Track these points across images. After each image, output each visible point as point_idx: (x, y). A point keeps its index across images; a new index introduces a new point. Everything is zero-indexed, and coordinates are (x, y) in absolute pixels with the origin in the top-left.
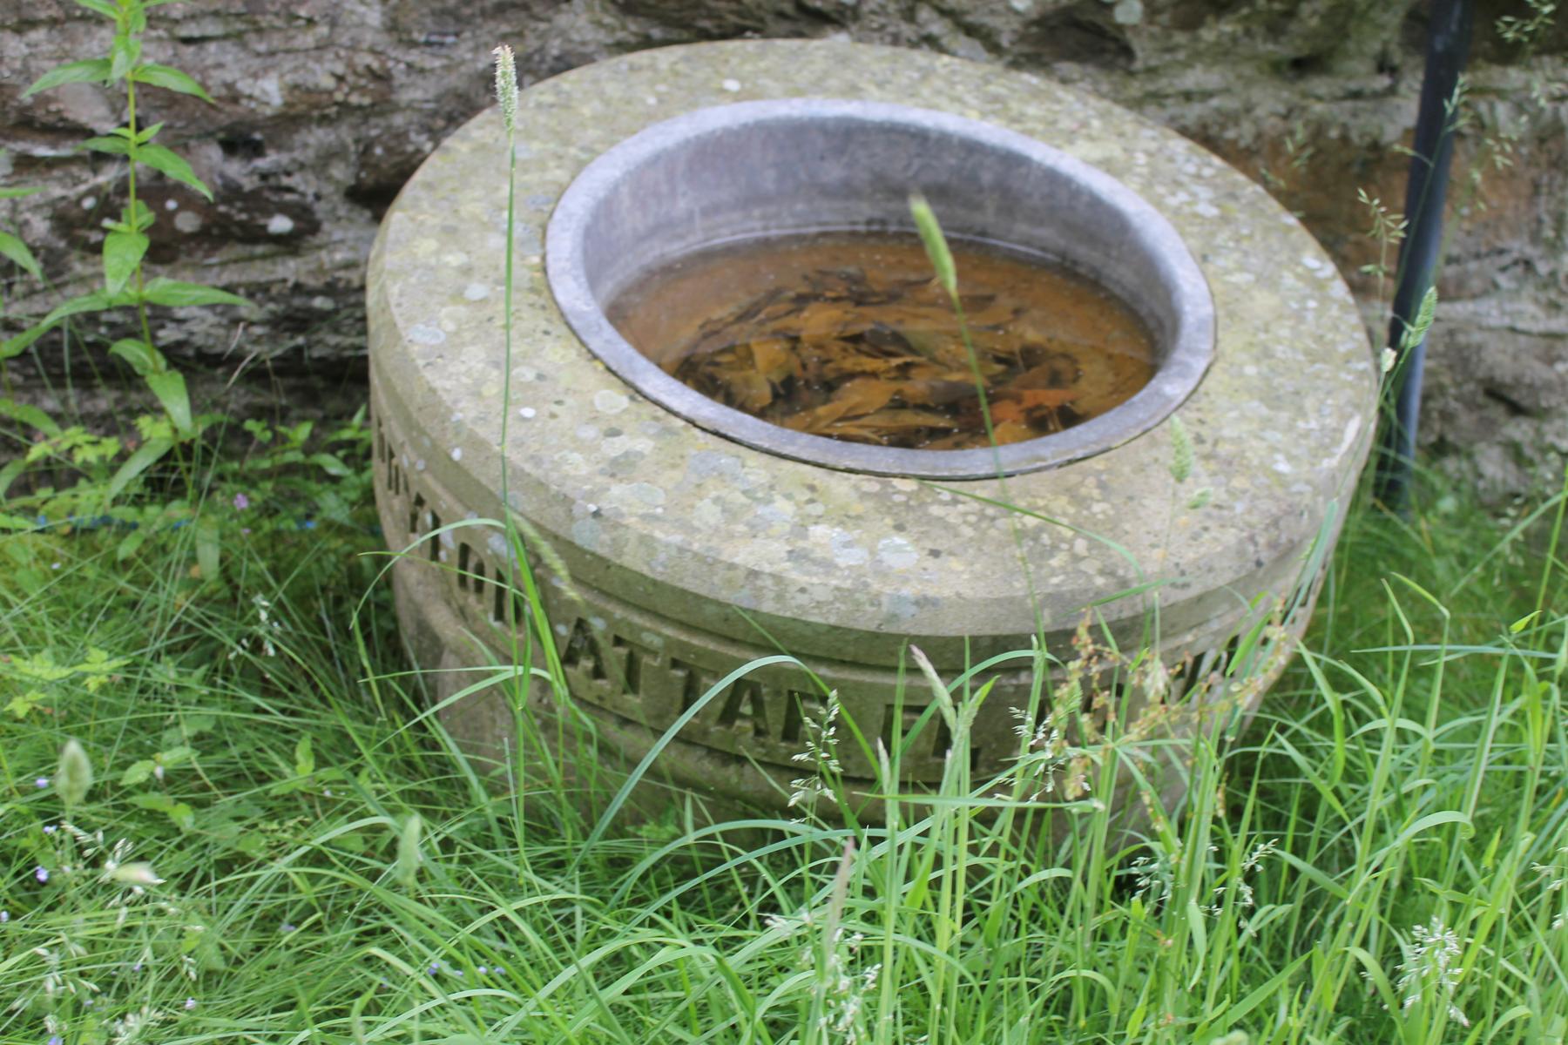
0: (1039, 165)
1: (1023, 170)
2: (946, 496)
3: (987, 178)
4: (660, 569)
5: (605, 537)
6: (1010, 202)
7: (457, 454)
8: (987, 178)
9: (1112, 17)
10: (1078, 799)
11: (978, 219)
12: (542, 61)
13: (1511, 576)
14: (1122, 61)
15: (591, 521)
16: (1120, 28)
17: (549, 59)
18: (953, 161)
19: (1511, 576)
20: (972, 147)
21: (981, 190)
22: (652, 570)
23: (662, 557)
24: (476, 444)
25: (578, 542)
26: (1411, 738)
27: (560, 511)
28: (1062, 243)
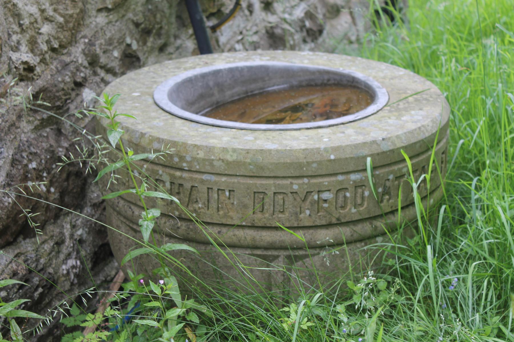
0: (225, 69)
1: (221, 74)
2: (409, 92)
3: (211, 83)
4: (405, 142)
5: (390, 143)
6: (221, 87)
7: (332, 157)
8: (211, 83)
9: (132, 49)
10: (440, 328)
11: (214, 99)
12: (24, 145)
13: (291, 260)
14: (137, 64)
15: (383, 142)
16: (135, 51)
17: (25, 143)
18: (200, 84)
19: (291, 260)
20: (204, 76)
21: (211, 89)
22: (404, 143)
23: (403, 138)
24: (335, 149)
25: (385, 150)
26: (452, 207)
27: (375, 146)
28: (244, 89)
